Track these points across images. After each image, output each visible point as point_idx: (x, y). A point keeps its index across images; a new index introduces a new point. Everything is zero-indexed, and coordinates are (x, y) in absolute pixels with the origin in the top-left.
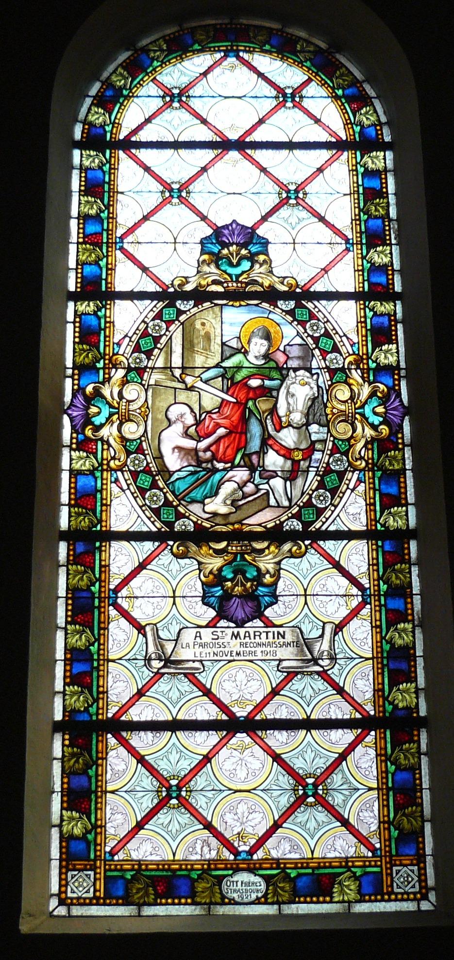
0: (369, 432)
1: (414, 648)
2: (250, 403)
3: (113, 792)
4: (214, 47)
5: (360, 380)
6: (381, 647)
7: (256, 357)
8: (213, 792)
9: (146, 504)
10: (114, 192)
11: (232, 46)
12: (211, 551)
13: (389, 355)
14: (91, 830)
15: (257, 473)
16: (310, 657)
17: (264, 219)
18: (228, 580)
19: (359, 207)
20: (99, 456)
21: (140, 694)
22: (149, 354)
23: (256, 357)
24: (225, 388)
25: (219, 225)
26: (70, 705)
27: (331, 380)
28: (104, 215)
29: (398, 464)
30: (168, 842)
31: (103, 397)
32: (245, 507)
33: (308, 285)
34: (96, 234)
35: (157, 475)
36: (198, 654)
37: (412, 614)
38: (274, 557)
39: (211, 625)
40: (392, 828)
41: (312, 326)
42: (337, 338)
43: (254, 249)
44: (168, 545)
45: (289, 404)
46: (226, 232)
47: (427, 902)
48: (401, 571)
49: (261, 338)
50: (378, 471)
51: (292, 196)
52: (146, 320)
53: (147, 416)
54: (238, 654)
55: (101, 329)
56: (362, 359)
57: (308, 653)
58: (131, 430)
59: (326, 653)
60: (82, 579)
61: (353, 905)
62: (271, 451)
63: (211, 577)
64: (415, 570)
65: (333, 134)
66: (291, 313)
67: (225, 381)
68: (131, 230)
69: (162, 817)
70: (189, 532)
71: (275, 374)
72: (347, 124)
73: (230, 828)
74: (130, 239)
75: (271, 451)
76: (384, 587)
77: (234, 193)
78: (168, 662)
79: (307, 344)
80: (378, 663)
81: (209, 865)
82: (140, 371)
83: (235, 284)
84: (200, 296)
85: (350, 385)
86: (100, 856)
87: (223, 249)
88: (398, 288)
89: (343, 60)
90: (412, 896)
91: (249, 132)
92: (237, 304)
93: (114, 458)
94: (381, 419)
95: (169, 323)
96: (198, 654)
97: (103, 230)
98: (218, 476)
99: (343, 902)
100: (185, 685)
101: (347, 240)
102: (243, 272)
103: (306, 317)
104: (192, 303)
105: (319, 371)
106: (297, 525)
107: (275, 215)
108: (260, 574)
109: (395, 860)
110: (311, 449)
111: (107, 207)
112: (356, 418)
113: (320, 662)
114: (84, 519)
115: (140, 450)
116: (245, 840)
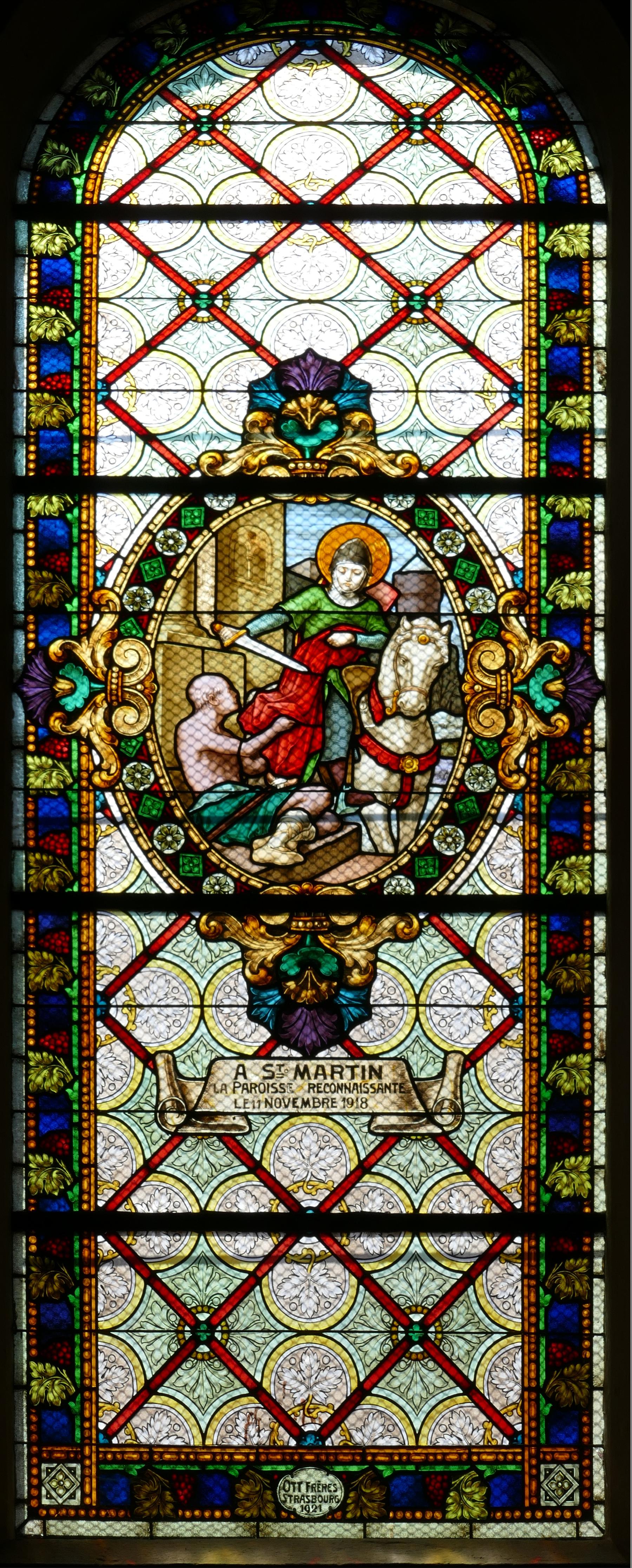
0: (535, 726)
1: (591, 1097)
2: (332, 675)
3: (107, 1332)
4: (277, 29)
5: (524, 636)
6: (538, 1094)
7: (343, 594)
8: (265, 1335)
9: (154, 848)
10: (91, 299)
11: (311, 27)
12: (263, 929)
13: (577, 592)
14: (75, 1395)
15: (342, 795)
16: (421, 1110)
17: (365, 347)
18: (291, 978)
19: (537, 324)
20: (74, 766)
21: (149, 1168)
22: (157, 588)
23: (343, 594)
24: (289, 646)
25: (283, 359)
26: (37, 1186)
27: (473, 634)
28: (74, 341)
29: (582, 781)
30: (194, 1415)
31: (79, 663)
32: (320, 853)
33: (437, 468)
34: (60, 372)
35: (172, 798)
36: (240, 1103)
37: (591, 1041)
38: (369, 939)
39: (262, 1054)
40: (543, 1401)
41: (443, 541)
42: (486, 560)
43: (344, 401)
44: (193, 918)
45: (398, 676)
46: (295, 371)
47: (590, 1524)
48: (576, 966)
49: (352, 560)
50: (546, 793)
51: (415, 304)
52: (151, 527)
53: (155, 696)
54: (306, 1103)
55: (72, 545)
56: (530, 597)
57: (417, 1102)
58: (127, 719)
59: (447, 1104)
60: (50, 974)
61: (477, 1525)
62: (365, 758)
63: (262, 973)
64: (600, 965)
65: (496, 189)
66: (407, 515)
67: (290, 636)
68: (124, 368)
69: (185, 1375)
70: (226, 896)
71: (377, 625)
72: (524, 171)
73: (291, 1391)
74: (121, 383)
75: (365, 758)
76: (546, 993)
77: (310, 298)
78: (192, 1115)
79: (434, 572)
80: (531, 1122)
81: (257, 1455)
82: (142, 619)
83: (308, 465)
84: (246, 485)
85: (504, 643)
86: (90, 1438)
87: (289, 401)
88: (600, 471)
89: (523, 52)
90: (568, 1514)
91: (341, 188)
92: (312, 500)
93: (98, 768)
94: (557, 703)
95: (192, 533)
96: (240, 1103)
97: (73, 367)
98: (276, 801)
99: (462, 1520)
100: (221, 1156)
101: (512, 384)
102: (324, 443)
103: (433, 523)
104: (232, 498)
105: (452, 618)
106: (407, 886)
107: (384, 341)
108: (344, 969)
109: (545, 1453)
110: (434, 754)
111: (80, 325)
112: (513, 701)
113: (438, 1119)
114: (51, 873)
115: (143, 755)
116: (314, 1414)
